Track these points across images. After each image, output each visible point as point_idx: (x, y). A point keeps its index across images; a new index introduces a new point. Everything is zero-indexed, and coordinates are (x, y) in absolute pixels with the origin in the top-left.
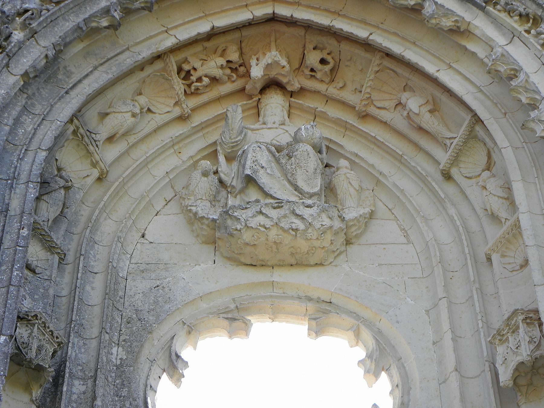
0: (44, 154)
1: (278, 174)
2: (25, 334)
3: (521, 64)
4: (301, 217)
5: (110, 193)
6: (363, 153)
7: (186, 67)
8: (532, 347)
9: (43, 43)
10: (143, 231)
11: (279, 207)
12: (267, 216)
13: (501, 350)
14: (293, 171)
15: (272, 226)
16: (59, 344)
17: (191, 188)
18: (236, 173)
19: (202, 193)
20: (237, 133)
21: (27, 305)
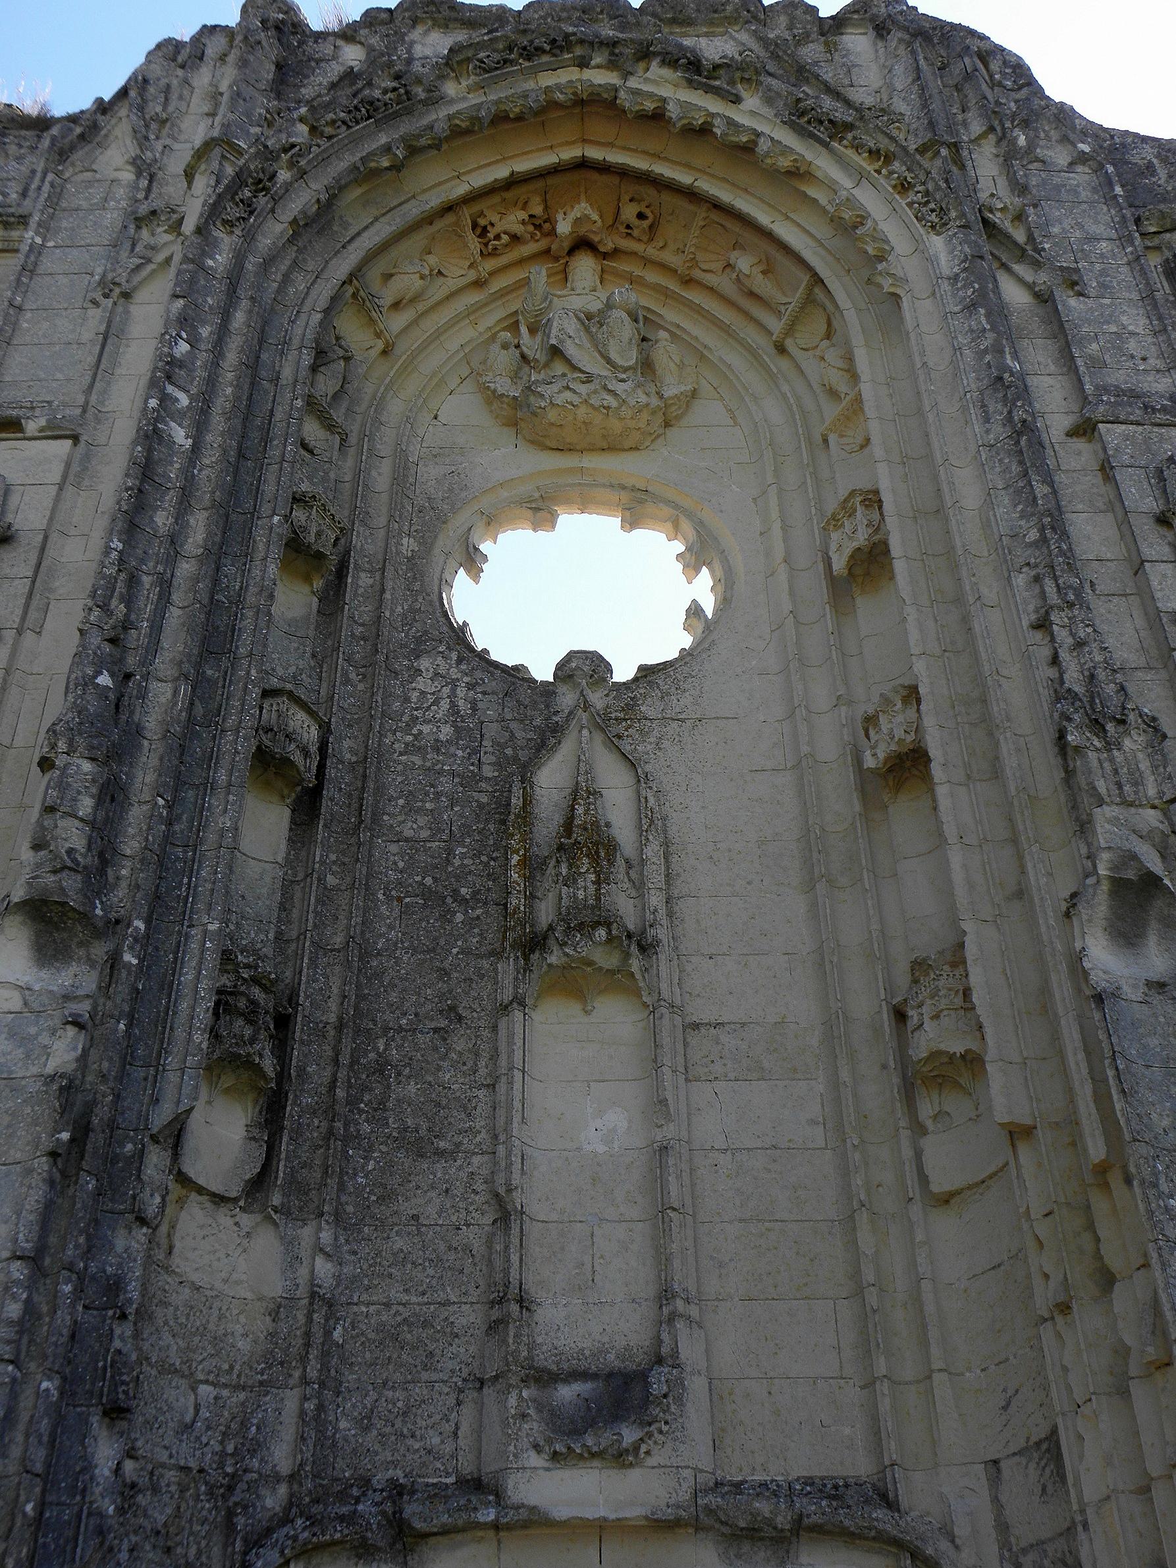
0: (319, 316)
2: (303, 518)
3: (869, 209)
5: (396, 367)
6: (686, 324)
7: (482, 222)
8: (870, 531)
9: (314, 186)
11: (588, 382)
12: (574, 392)
13: (835, 536)
16: (342, 529)
17: (489, 363)
21: (305, 487)
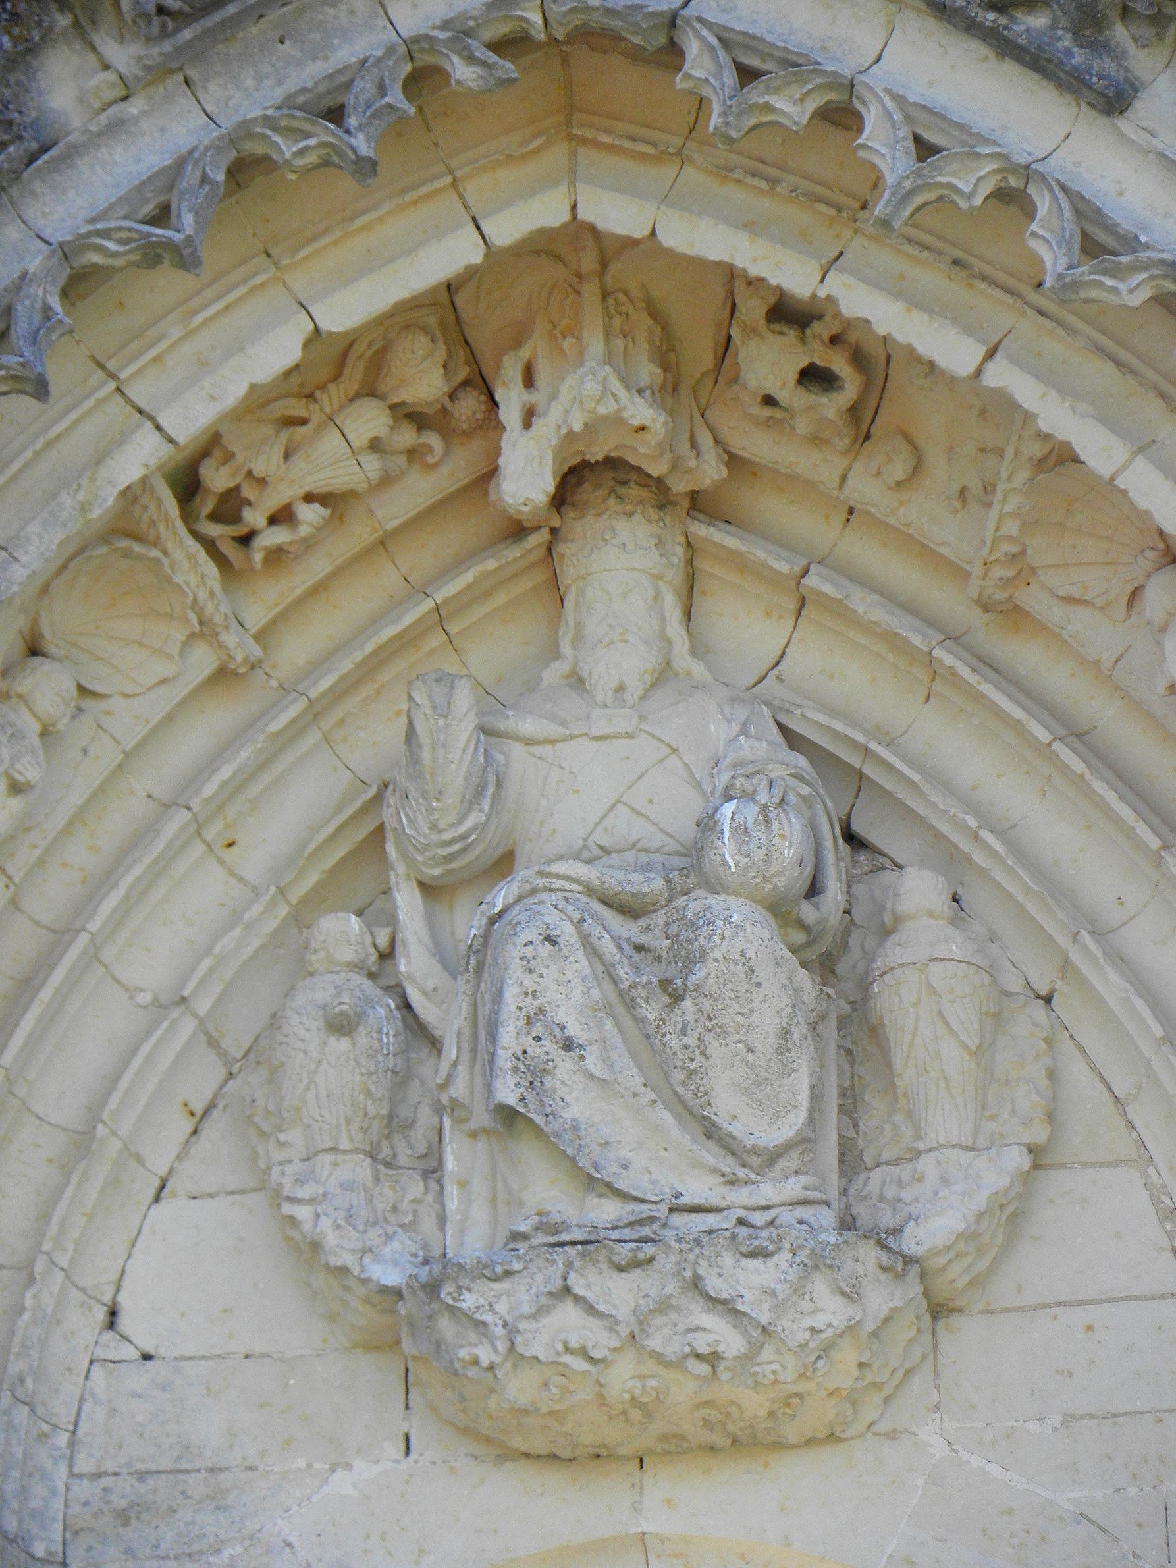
1: (632, 1078)
4: (726, 1307)
10: (107, 1298)
14: (692, 1060)
15: (615, 1350)
18: (467, 1032)
19: (334, 1122)
20: (462, 802)
